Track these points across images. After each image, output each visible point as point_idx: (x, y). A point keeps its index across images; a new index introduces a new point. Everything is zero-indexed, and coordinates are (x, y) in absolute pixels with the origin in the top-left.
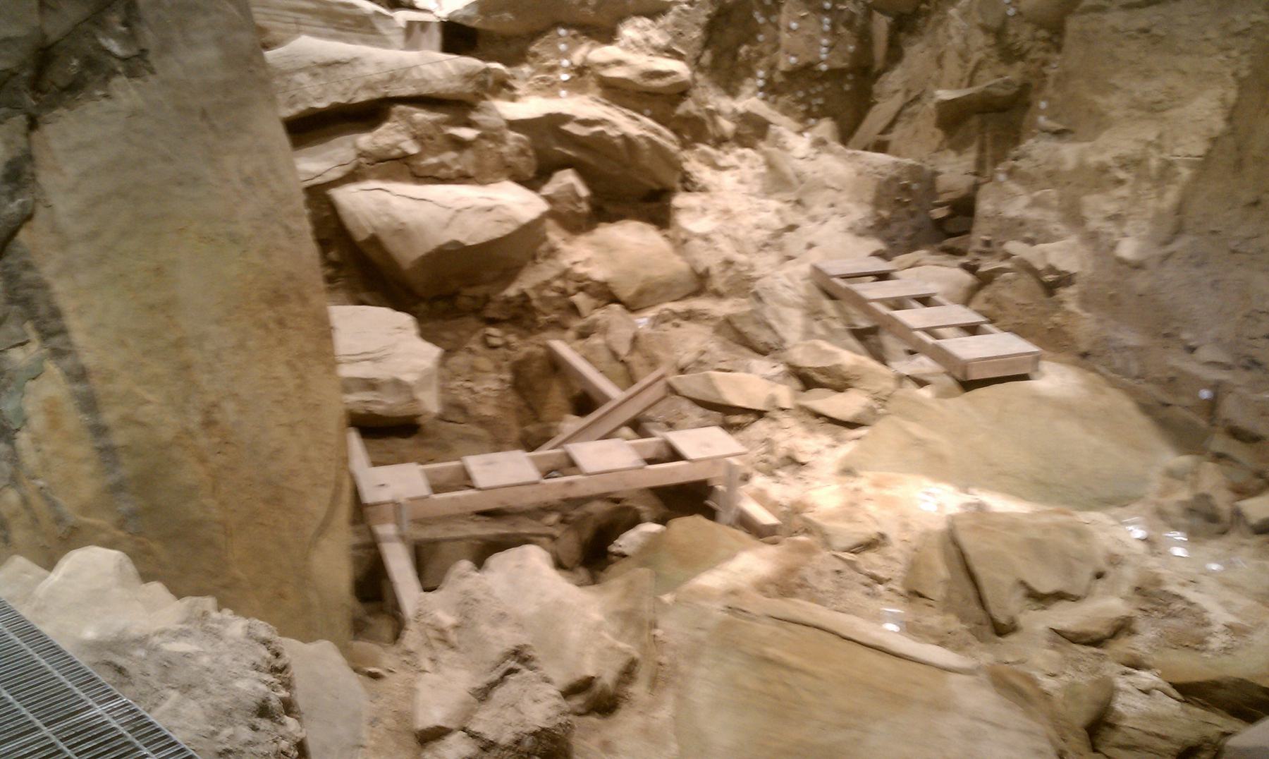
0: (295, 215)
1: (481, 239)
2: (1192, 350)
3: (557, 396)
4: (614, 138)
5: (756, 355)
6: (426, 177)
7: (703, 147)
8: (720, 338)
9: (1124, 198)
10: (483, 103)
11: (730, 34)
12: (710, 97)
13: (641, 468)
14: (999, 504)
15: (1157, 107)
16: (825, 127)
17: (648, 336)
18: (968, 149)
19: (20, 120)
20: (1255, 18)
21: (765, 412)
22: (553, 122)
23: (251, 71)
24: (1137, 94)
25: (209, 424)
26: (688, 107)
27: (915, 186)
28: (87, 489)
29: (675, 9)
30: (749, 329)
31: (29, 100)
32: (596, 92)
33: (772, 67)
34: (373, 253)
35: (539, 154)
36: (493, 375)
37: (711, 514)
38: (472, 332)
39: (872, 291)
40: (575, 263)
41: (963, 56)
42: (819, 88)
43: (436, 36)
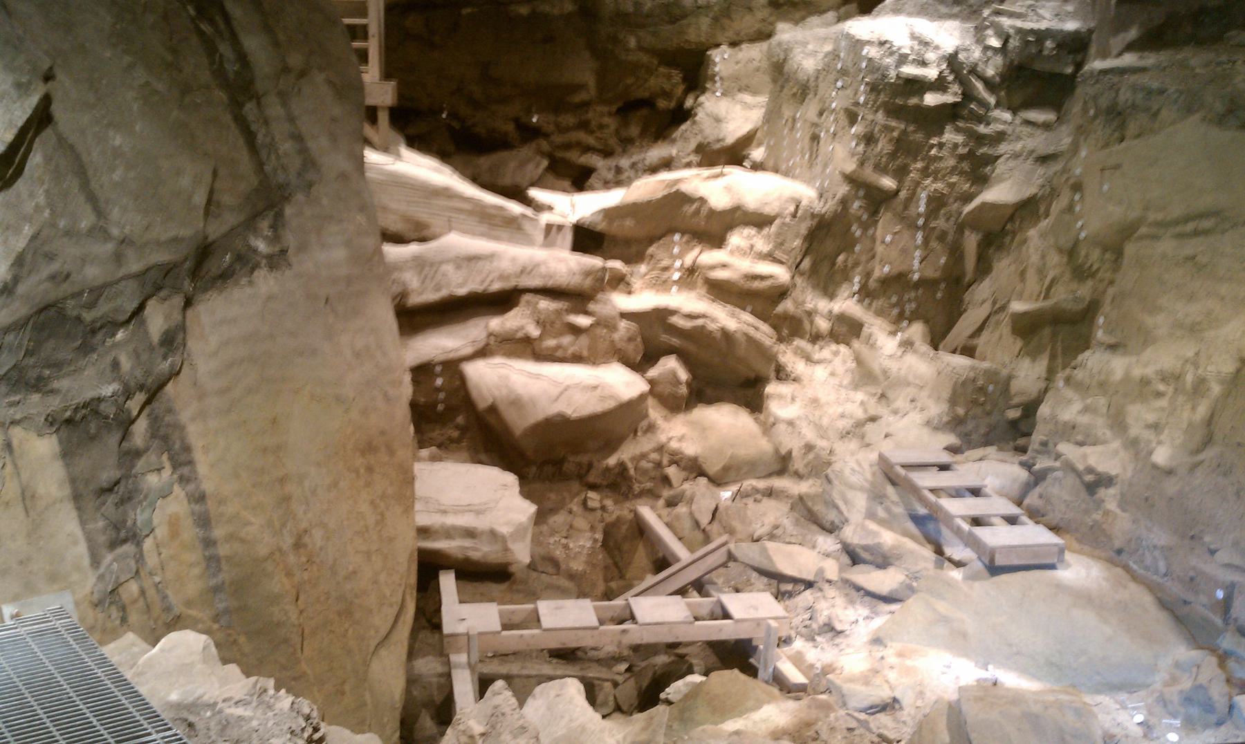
2: (1212, 552)
3: (641, 557)
8: (796, 515)
9: (1163, 409)
11: (829, 245)
13: (691, 623)
14: (1011, 680)
16: (917, 330)
17: (727, 508)
19: (178, 301)
21: (815, 582)
22: (661, 316)
24: (1180, 315)
25: (298, 545)
28: (193, 587)
29: (777, 222)
30: (819, 508)
31: (188, 286)
33: (868, 275)
34: (491, 420)
35: (645, 341)
37: (752, 671)
39: (925, 480)
40: (670, 439)
41: (1041, 272)
42: (913, 294)
43: (568, 237)
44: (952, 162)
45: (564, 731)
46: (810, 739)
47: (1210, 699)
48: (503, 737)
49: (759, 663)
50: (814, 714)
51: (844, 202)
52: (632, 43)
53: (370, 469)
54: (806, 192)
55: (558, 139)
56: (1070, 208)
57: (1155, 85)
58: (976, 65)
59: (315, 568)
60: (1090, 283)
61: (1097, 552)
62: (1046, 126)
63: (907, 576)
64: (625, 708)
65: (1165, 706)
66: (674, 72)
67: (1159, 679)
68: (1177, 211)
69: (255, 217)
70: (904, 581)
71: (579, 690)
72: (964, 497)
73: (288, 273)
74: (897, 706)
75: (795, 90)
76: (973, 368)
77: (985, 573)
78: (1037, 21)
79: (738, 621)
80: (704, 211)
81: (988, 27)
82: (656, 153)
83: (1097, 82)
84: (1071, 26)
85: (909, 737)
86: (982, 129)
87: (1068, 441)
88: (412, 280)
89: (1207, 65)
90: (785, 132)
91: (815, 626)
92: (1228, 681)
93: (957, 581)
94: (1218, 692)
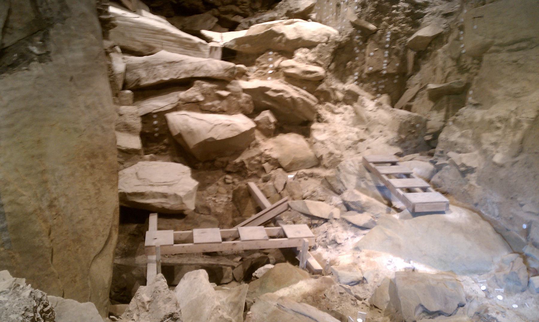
2: (522, 205)
3: (250, 206)
4: (286, 98)
5: (336, 195)
6: (206, 111)
8: (324, 186)
10: (233, 81)
11: (344, 57)
13: (267, 240)
14: (422, 268)
15: (518, 95)
17: (291, 183)
18: (441, 111)
22: (262, 90)
27: (418, 125)
29: (319, 45)
30: (334, 183)
32: (282, 79)
33: (362, 71)
34: (179, 140)
35: (255, 103)
36: (226, 195)
37: (295, 262)
38: (220, 177)
39: (384, 170)
41: (443, 69)
42: (383, 81)
43: (219, 53)
45: (196, 297)
46: (321, 298)
47: (519, 279)
48: (159, 303)
49: (300, 258)
50: (324, 285)
51: (351, 36)
53: (93, 166)
54: (333, 31)
55: (222, 9)
59: (60, 217)
60: (466, 75)
61: (465, 205)
63: (372, 217)
64: (237, 279)
65: (497, 281)
67: (493, 269)
68: (509, 38)
69: (33, 34)
70: (371, 219)
71: (205, 276)
72: (402, 178)
73: (50, 64)
74: (365, 281)
76: (409, 116)
77: (410, 216)
79: (290, 239)
82: (268, 15)
85: (370, 297)
87: (453, 151)
91: (328, 241)
92: (528, 269)
93: (396, 219)
94: (523, 275)
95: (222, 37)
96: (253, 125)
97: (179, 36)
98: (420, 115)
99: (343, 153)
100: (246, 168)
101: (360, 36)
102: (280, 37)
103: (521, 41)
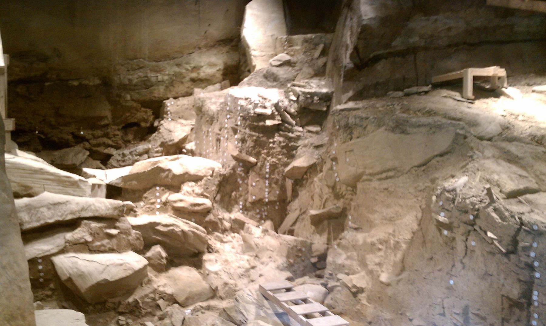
0: (24, 280)
1: (117, 278)
2: (411, 320)
4: (176, 232)
6: (76, 244)
7: (217, 234)
9: (382, 256)
10: (122, 218)
11: (228, 188)
12: (220, 213)
16: (268, 224)
17: (189, 318)
20: (426, 185)
22: (152, 226)
23: (10, 220)
24: (385, 214)
26: (211, 217)
27: (304, 249)
29: (205, 178)
30: (233, 314)
32: (171, 213)
33: (246, 200)
34: (69, 285)
39: (283, 297)
40: (158, 286)
41: (321, 196)
42: (265, 208)
43: (104, 191)
44: (279, 149)
51: (234, 169)
52: (128, 97)
54: (217, 166)
55: (94, 142)
56: (331, 169)
57: (364, 115)
58: (286, 107)
60: (342, 200)
62: (317, 133)
66: (148, 110)
68: (378, 169)
75: (208, 119)
78: (310, 89)
80: (170, 176)
81: (290, 92)
82: (142, 147)
83: (340, 114)
84: (324, 90)
86: (290, 135)
87: (342, 273)
88: (24, 216)
89: (383, 107)
90: (204, 137)
95: (106, 175)
96: (146, 262)
97: (59, 175)
98: (304, 239)
99: (237, 283)
100: (141, 307)
101: (242, 169)
102: (166, 173)
103: (388, 170)
